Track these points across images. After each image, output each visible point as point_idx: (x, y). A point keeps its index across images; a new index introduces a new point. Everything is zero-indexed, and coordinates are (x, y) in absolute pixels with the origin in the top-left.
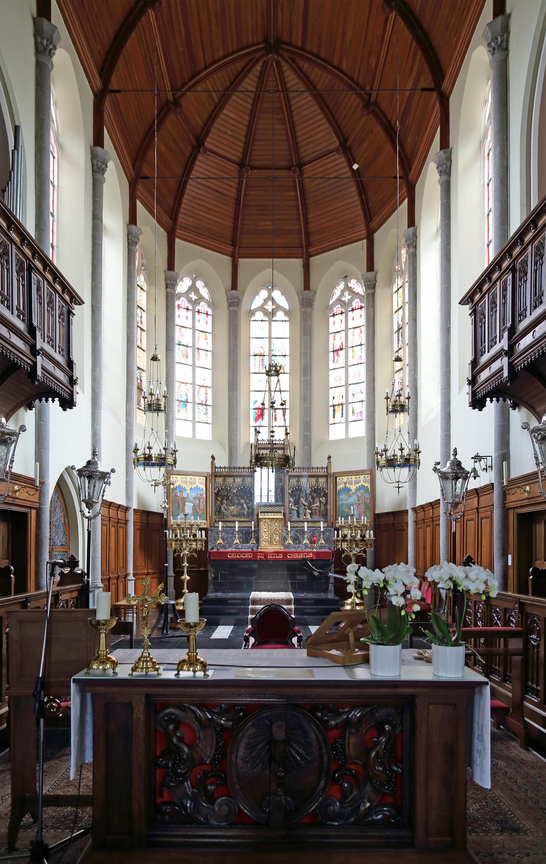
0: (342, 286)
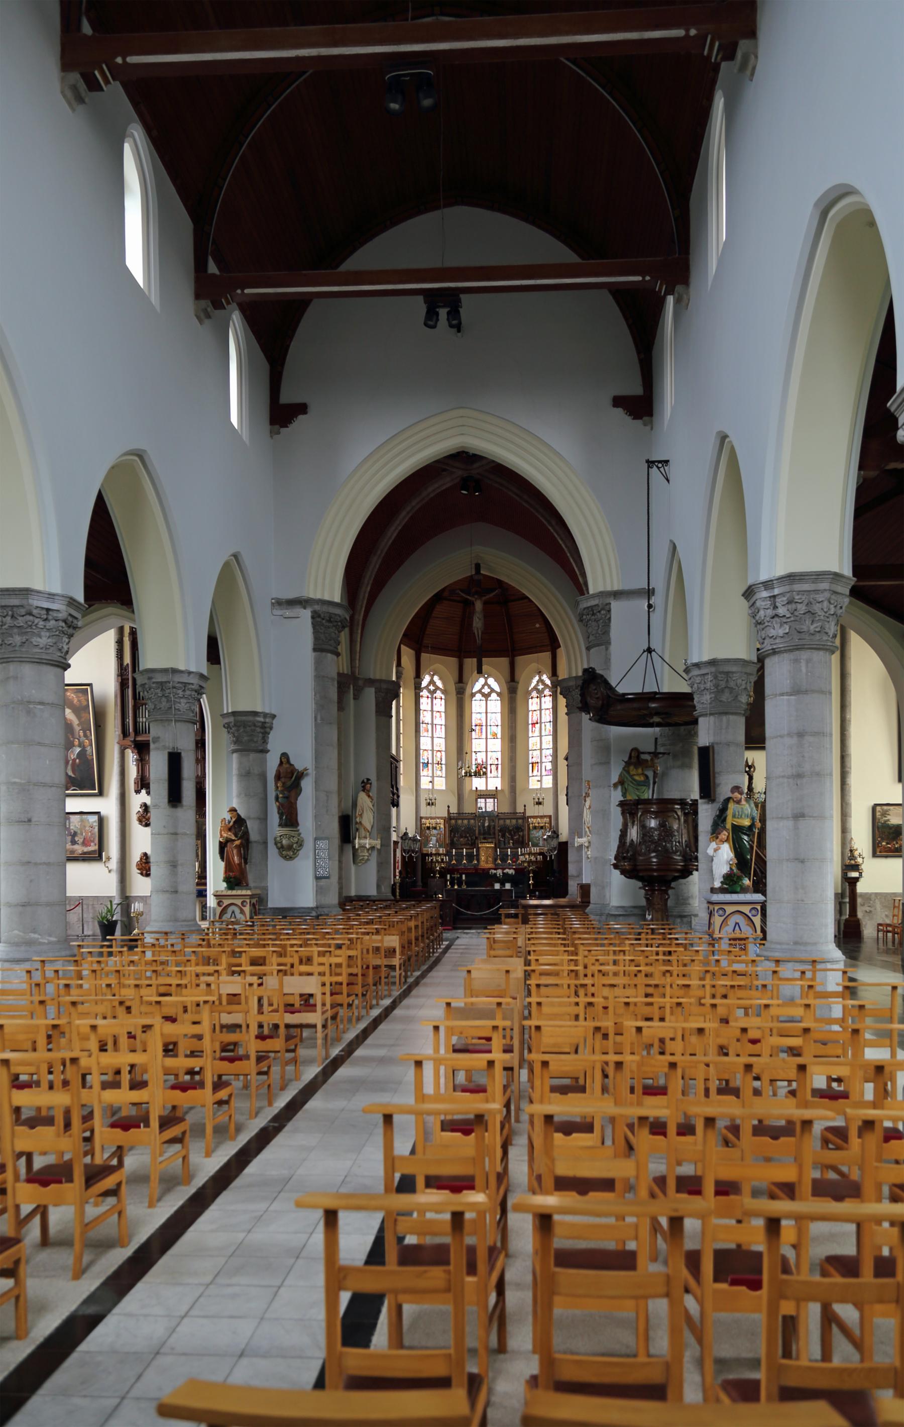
0: (537, 678)
